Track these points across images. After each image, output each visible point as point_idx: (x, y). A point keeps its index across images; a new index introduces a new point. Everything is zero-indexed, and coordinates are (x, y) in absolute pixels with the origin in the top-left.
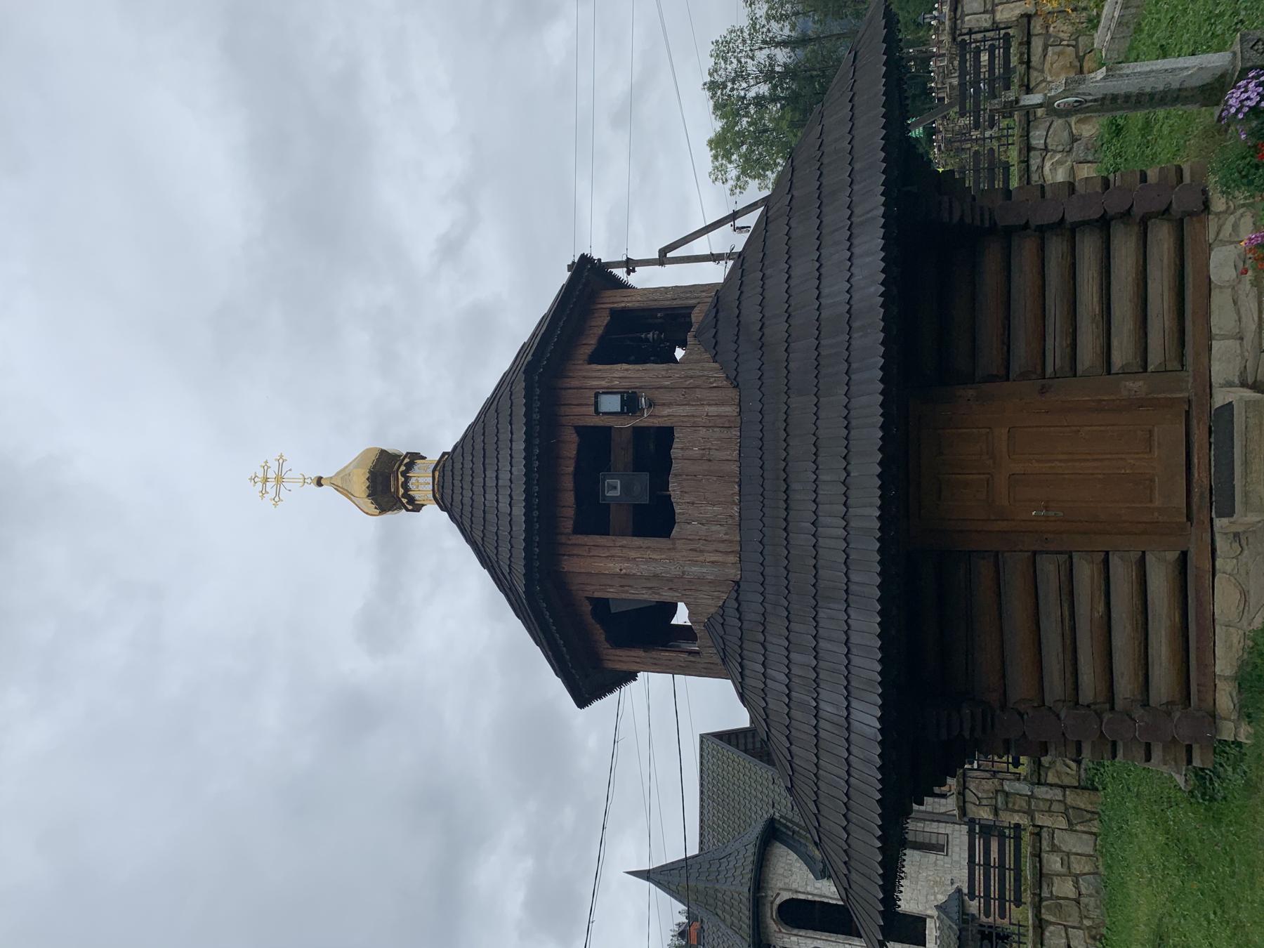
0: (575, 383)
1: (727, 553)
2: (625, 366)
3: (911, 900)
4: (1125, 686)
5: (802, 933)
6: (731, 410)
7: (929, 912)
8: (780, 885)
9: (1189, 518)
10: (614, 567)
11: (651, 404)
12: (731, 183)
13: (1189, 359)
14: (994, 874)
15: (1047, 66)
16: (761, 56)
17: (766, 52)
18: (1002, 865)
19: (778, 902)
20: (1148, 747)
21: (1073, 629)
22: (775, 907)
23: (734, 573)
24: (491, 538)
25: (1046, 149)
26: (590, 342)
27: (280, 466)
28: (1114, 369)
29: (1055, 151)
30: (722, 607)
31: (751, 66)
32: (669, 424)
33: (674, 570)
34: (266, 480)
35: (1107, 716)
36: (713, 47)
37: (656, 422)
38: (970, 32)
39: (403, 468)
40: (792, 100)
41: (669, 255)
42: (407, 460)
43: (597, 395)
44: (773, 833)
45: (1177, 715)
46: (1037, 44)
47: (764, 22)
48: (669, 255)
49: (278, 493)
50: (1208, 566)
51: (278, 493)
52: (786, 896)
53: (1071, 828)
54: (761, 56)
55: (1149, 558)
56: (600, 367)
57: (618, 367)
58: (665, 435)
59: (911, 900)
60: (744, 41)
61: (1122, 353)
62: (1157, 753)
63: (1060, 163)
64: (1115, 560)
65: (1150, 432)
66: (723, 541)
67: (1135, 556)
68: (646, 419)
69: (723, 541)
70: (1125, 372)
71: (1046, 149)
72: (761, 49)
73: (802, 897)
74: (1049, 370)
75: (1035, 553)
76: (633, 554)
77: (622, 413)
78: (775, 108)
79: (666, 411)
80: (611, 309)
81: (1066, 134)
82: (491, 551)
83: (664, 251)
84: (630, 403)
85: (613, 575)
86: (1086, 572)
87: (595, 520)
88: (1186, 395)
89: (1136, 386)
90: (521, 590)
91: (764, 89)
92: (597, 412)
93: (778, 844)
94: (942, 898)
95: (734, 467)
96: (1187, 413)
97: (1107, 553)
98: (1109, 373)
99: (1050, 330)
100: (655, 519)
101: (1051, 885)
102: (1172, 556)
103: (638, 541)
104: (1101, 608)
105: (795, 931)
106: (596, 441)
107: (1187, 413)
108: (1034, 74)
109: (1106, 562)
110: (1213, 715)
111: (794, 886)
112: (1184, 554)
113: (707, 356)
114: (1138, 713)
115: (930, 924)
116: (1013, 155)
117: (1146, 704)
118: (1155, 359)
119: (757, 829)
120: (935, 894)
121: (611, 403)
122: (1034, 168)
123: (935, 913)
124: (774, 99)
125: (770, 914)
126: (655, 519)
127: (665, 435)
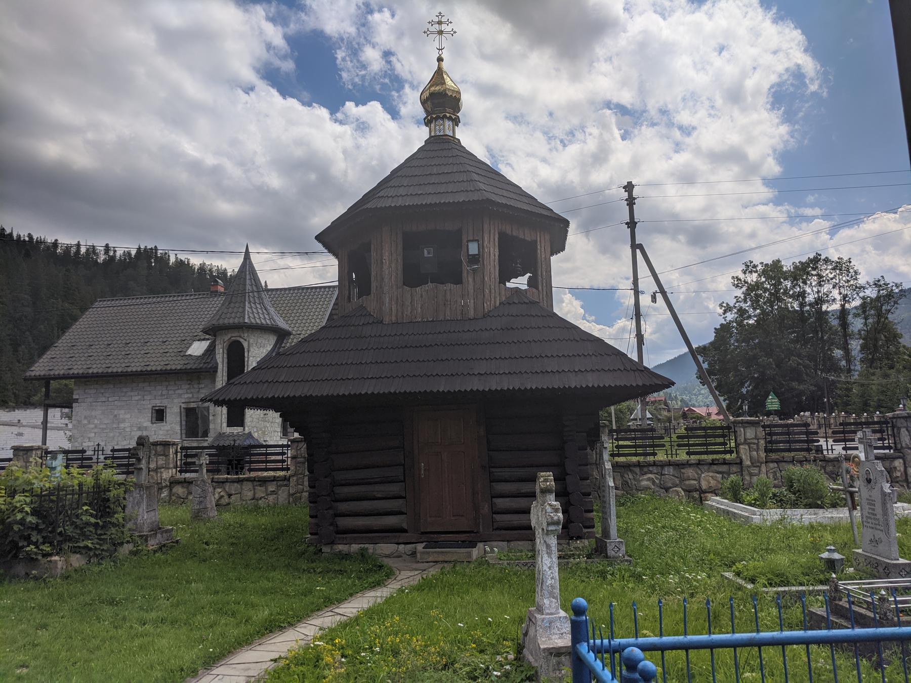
0: (486, 226)
1: (396, 316)
2: (497, 254)
3: (252, 416)
4: (343, 507)
5: (225, 356)
6: (472, 314)
7: (246, 428)
8: (251, 341)
9: (422, 533)
10: (386, 256)
11: (474, 270)
12: (742, 276)
13: (498, 532)
14: (263, 458)
15: (711, 474)
16: (835, 293)
17: (838, 297)
18: (267, 462)
19: (241, 340)
20: (316, 517)
21: (370, 484)
22: (238, 339)
23: (386, 320)
24: (392, 192)
25: (662, 475)
26: (508, 229)
27: (448, 33)
28: (494, 499)
29: (660, 480)
30: (370, 314)
31: (826, 288)
32: (464, 281)
33: (386, 289)
34: (440, 23)
35: (328, 499)
36: (845, 259)
37: (465, 275)
38: (735, 432)
39: (448, 115)
40: (801, 316)
41: (638, 251)
42: (454, 117)
43: (477, 241)
44: (282, 335)
45: (332, 528)
46: (724, 468)
47: (861, 294)
48: (638, 251)
49: (432, 33)
50: (400, 541)
51: (432, 33)
52: (245, 345)
53: (290, 495)
54: (835, 293)
55: (403, 516)
56: (497, 239)
57: (497, 250)
58: (458, 279)
59: (252, 416)
60: (848, 281)
61: (501, 503)
62: (313, 520)
63: (654, 483)
64: (401, 501)
65: (462, 516)
66: (402, 314)
67: (404, 510)
68: (466, 268)
69: (402, 314)
70: (492, 505)
71: (662, 475)
72: (840, 294)
73: (246, 355)
74: (493, 470)
75: (404, 465)
76: (393, 266)
77: (469, 255)
78: (796, 306)
79: (471, 280)
80: (536, 241)
81: (670, 485)
82: (399, 174)
83: (641, 247)
84: (474, 259)
85: (382, 256)
86: (394, 489)
87: (411, 244)
88: (481, 530)
89: (486, 509)
90: (369, 206)
91: (810, 298)
92: (468, 241)
93: (275, 338)
94: (256, 435)
95: (441, 318)
96: (472, 532)
97: (404, 498)
98: (492, 497)
99: (514, 470)
100: (413, 276)
101: (260, 486)
102: (405, 526)
103: (400, 268)
104: (379, 496)
105: (225, 351)
106: (456, 241)
107: (472, 532)
108: (706, 467)
109: (400, 497)
110: (333, 543)
111: (252, 349)
112: (405, 531)
113: (504, 299)
114: (331, 512)
115: (240, 429)
116: (661, 457)
117: (336, 515)
118: (498, 517)
119: (282, 324)
120: (257, 431)
121: (473, 249)
122: (651, 468)
123: (247, 431)
124: (802, 305)
125: (232, 336)
126: (413, 276)
127: (458, 279)
